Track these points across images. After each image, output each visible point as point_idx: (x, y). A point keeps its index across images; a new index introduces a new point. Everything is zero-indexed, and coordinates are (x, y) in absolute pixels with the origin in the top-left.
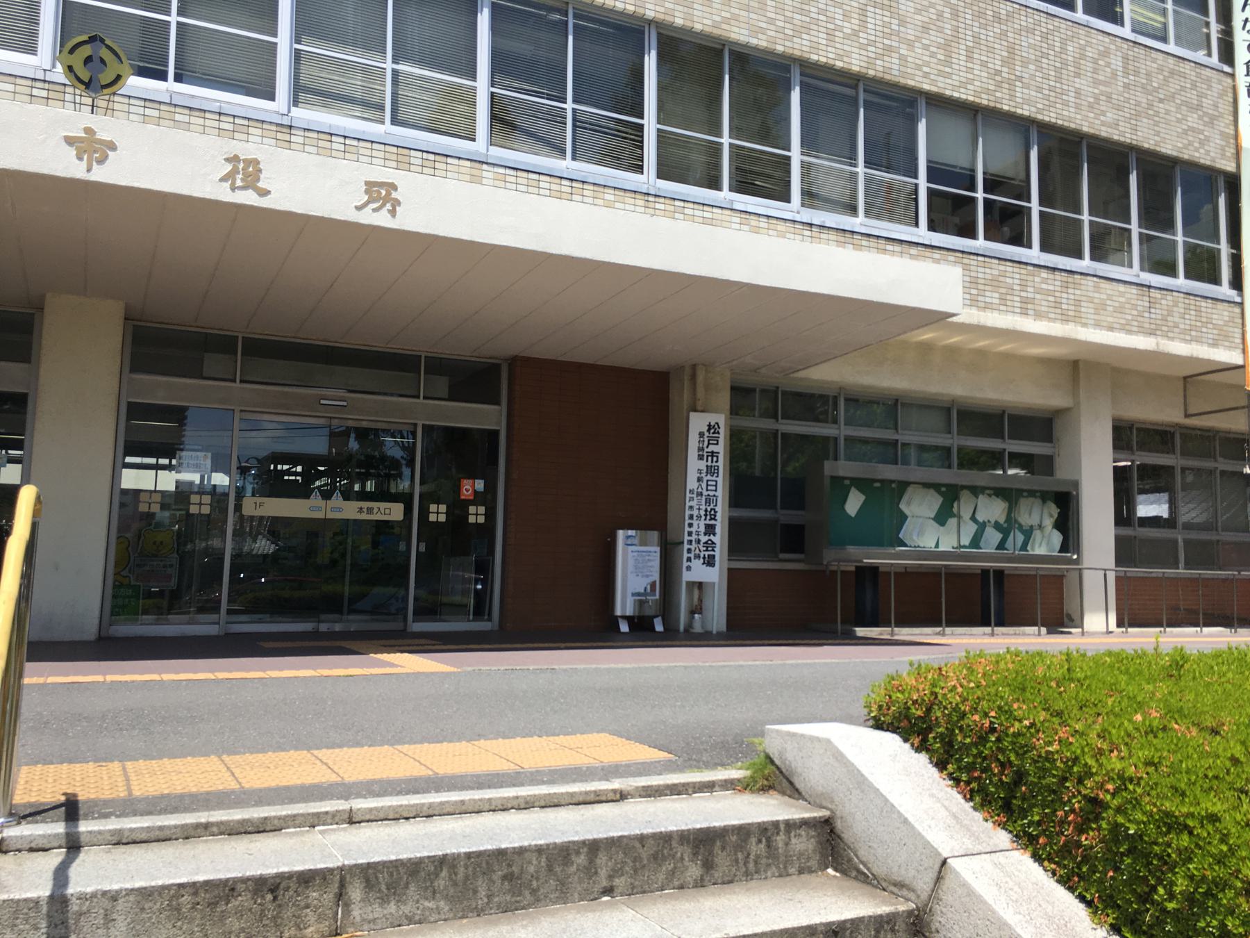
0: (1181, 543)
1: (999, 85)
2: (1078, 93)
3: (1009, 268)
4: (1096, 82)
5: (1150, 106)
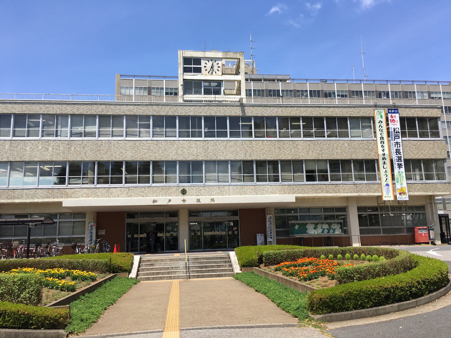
0: (381, 229)
1: (319, 155)
2: (337, 153)
3: (323, 186)
4: (341, 150)
5: (355, 151)
